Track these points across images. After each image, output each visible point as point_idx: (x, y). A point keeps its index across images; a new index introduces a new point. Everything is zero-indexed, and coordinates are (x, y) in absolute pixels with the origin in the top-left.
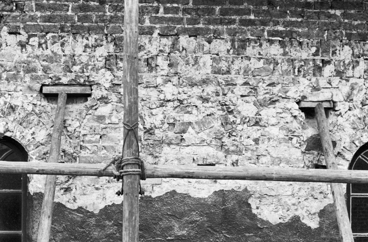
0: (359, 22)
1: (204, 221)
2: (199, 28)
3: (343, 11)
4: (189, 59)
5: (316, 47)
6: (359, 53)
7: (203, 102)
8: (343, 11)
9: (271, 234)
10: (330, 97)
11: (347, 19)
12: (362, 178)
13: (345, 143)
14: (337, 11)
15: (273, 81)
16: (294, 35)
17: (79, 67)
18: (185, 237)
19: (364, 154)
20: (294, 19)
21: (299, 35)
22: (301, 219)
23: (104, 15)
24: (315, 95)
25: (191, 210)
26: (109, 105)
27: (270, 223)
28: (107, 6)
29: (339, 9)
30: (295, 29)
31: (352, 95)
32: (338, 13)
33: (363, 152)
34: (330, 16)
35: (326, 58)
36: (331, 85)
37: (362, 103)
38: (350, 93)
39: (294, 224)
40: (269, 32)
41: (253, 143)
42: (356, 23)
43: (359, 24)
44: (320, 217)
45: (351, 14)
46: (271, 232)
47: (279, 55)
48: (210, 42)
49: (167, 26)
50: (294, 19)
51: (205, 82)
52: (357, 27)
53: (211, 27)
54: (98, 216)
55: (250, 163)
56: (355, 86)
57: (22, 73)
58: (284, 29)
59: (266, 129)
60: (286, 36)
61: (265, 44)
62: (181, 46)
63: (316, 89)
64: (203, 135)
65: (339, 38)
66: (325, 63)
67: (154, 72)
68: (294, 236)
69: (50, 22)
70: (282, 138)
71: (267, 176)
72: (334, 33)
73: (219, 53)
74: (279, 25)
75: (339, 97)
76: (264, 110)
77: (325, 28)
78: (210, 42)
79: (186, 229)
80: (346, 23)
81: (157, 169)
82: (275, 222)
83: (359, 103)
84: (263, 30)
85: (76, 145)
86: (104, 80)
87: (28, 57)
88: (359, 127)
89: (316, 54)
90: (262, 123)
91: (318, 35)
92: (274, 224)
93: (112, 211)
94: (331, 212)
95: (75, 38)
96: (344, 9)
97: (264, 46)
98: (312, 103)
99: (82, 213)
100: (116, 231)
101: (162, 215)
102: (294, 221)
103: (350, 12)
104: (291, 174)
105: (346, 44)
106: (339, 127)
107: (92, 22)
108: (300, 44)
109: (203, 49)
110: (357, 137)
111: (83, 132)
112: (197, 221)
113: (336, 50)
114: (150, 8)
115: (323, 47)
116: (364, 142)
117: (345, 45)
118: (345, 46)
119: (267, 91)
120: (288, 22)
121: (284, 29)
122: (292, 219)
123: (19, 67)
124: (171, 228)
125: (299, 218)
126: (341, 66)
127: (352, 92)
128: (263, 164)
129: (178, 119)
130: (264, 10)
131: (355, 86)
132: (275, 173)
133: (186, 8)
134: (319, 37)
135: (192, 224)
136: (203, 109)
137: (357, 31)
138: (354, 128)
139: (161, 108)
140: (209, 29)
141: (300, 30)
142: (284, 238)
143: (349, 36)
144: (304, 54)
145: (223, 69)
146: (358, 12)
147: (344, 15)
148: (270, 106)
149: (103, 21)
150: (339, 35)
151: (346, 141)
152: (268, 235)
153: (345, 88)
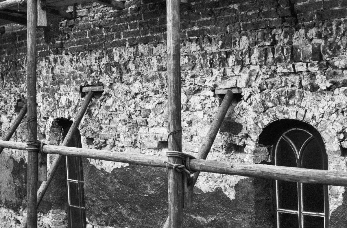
0: (253, 12)
1: (163, 185)
2: (148, 37)
3: (239, 4)
4: (145, 61)
5: (222, 40)
6: (253, 42)
7: (155, 94)
8: (239, 4)
9: (203, 200)
10: (235, 84)
11: (244, 11)
12: (137, 160)
13: (250, 125)
14: (235, 5)
15: (194, 74)
16: (205, 33)
17: (95, 73)
18: (154, 195)
19: (286, 135)
20: (205, 19)
21: (209, 32)
22: (223, 190)
23: (102, 36)
24: (224, 83)
25: (156, 176)
26: (111, 98)
27: (202, 192)
28: (103, 29)
29: (236, 3)
30: (206, 27)
31: (251, 82)
32: (236, 6)
33: (283, 133)
34: (230, 11)
35: (228, 50)
36: (234, 73)
37: (259, 88)
38: (248, 79)
39: (218, 194)
40: (188, 33)
41: (187, 125)
42: (250, 14)
43: (253, 14)
44: (236, 190)
45: (246, 6)
46: (203, 198)
47: (197, 51)
48: (156, 46)
49: (132, 38)
50: (205, 19)
51: (154, 78)
52: (251, 17)
53: (155, 35)
54: (110, 175)
55: (187, 141)
56: (253, 73)
57: (72, 80)
58: (198, 29)
59: (195, 113)
60: (200, 34)
61: (187, 44)
62: (140, 52)
63: (224, 77)
64: (158, 119)
65: (237, 30)
66: (228, 54)
67: (129, 73)
68: (219, 204)
69: (79, 45)
70: (206, 121)
71: (90, 155)
72: (233, 26)
73: (161, 55)
74: (195, 26)
75: (242, 84)
76: (192, 98)
77: (227, 22)
78: (156, 46)
79: (154, 190)
80: (242, 15)
81: (47, 148)
82: (206, 191)
83: (257, 88)
84: (185, 32)
85: (98, 126)
86: (105, 81)
87: (73, 69)
88: (260, 110)
89: (222, 47)
90: (191, 109)
91: (221, 31)
92: (205, 192)
93: (117, 172)
94: (243, 187)
95: (91, 54)
96: (239, 2)
97: (187, 45)
98: (223, 90)
99: (103, 173)
100: (119, 187)
101: (142, 178)
102: (218, 191)
103: (244, 4)
104: (101, 155)
105: (244, 35)
106: (244, 111)
107: (97, 42)
108: (210, 40)
109: (152, 52)
110: (260, 120)
111: (101, 117)
112: (159, 184)
113: (236, 41)
114: (123, 26)
115: (228, 41)
116: (265, 124)
117: (243, 35)
118: (243, 36)
119: (190, 82)
120: (201, 22)
121: (198, 29)
122: (216, 190)
123: (70, 76)
124: (146, 188)
125: (221, 189)
126: (240, 56)
127: (250, 79)
128: (195, 142)
129: (142, 107)
130: (185, 15)
131: (252, 72)
132: (93, 153)
133: (141, 23)
134: (222, 31)
135: (157, 186)
136: (155, 99)
137: (252, 21)
138: (256, 112)
139: (133, 99)
140: (153, 37)
141: (209, 28)
142: (212, 205)
143: (245, 27)
144: (213, 49)
145: (164, 66)
146: (251, 3)
147: (241, 8)
148: (195, 95)
149: (102, 40)
150: (237, 27)
151: (251, 124)
152: (201, 201)
153: (245, 76)
